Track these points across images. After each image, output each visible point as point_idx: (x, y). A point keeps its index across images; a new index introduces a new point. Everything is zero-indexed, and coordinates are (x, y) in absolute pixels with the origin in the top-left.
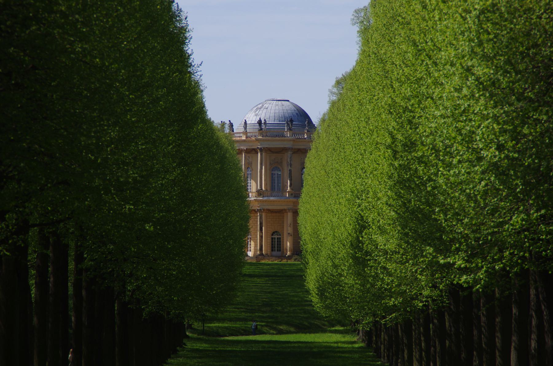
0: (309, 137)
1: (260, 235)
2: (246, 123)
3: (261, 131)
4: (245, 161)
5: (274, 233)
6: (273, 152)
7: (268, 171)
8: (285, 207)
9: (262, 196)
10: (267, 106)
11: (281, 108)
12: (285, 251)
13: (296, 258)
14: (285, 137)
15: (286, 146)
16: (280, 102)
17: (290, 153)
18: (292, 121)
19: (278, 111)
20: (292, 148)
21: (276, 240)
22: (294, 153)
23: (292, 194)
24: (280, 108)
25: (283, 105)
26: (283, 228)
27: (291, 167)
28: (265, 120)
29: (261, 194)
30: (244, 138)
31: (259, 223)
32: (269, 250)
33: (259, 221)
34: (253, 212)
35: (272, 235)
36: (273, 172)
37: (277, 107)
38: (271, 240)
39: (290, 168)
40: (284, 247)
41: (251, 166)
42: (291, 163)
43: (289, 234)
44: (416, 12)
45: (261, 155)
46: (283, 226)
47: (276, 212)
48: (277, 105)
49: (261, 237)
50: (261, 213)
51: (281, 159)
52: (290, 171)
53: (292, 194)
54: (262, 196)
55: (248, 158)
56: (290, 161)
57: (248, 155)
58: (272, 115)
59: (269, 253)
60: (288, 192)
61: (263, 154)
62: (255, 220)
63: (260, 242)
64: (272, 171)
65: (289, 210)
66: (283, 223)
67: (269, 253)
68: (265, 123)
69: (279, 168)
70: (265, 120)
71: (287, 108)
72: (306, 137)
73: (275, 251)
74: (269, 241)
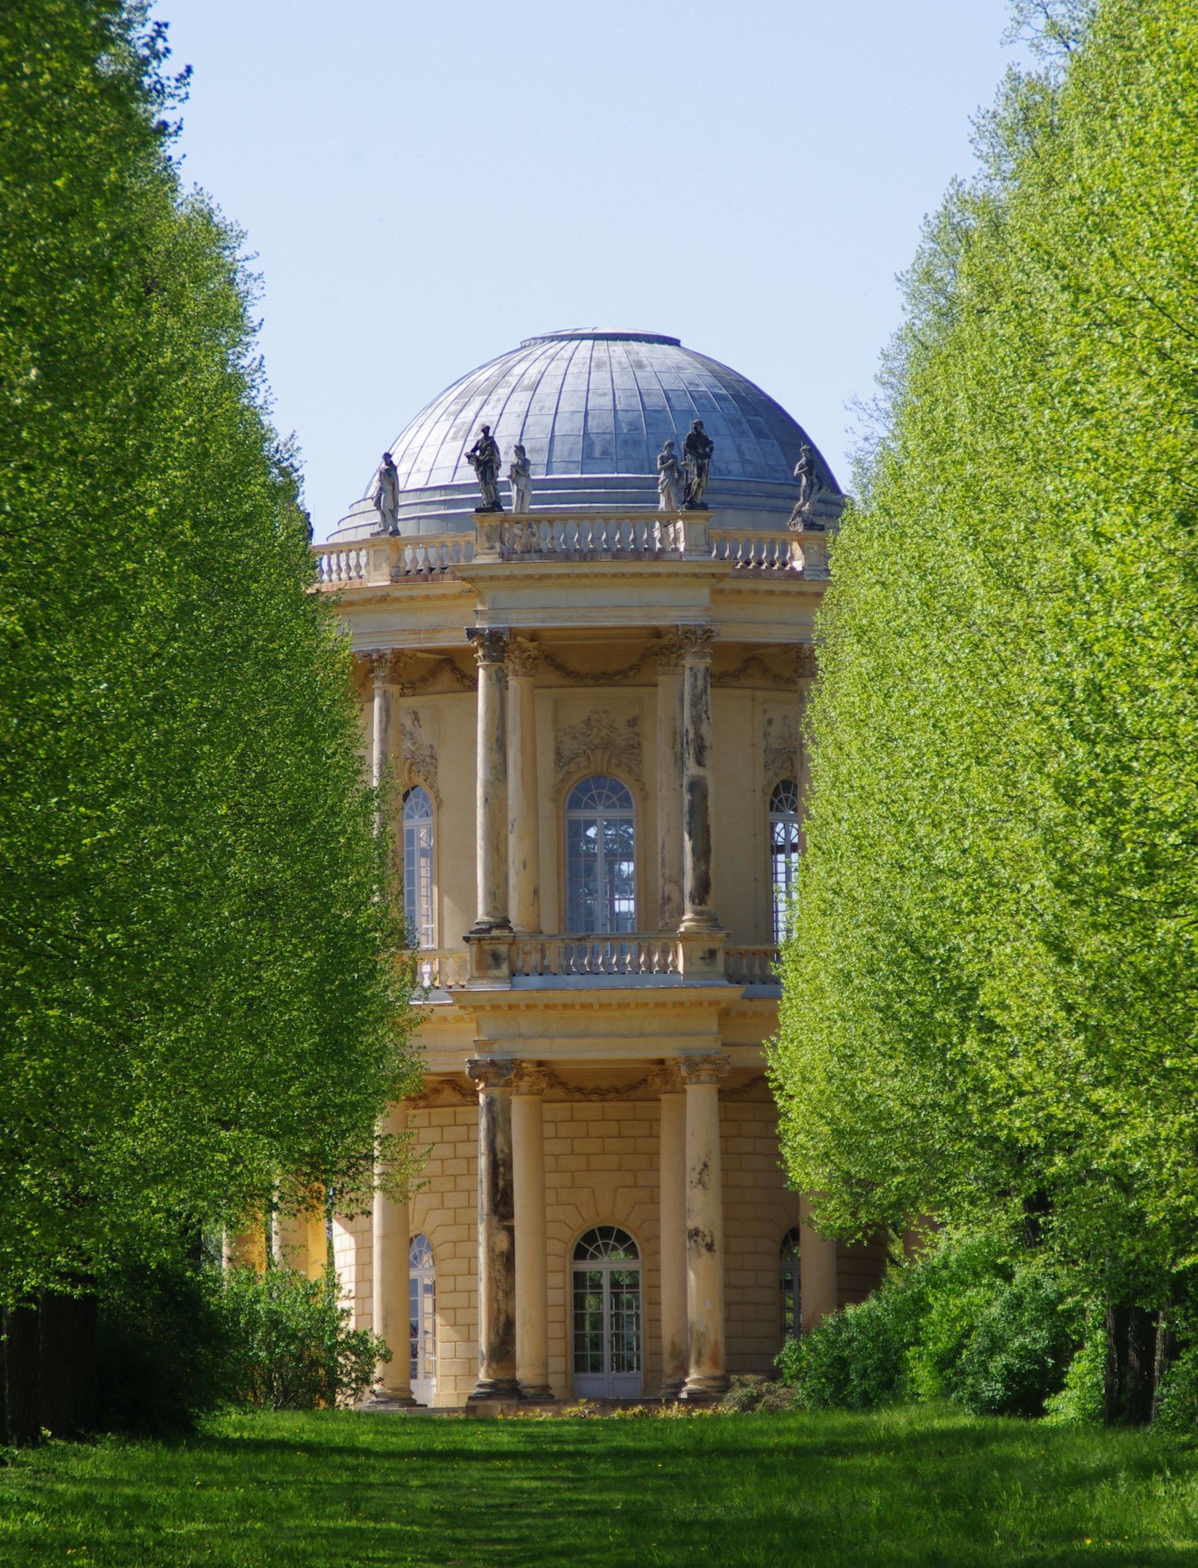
0: (819, 568)
1: (491, 1250)
2: (389, 472)
3: (493, 519)
4: (384, 741)
5: (589, 1237)
6: (575, 677)
7: (547, 808)
8: (668, 1050)
9: (505, 969)
10: (534, 372)
11: (631, 384)
12: (668, 1366)
13: (752, 1390)
14: (658, 556)
15: (663, 621)
16: (618, 348)
17: (694, 663)
18: (699, 444)
19: (607, 402)
20: (708, 634)
21: (607, 1353)
22: (718, 679)
23: (712, 954)
24: (624, 382)
25: (640, 365)
26: (654, 1201)
27: (700, 762)
28: (520, 450)
29: (496, 958)
30: (379, 580)
31: (483, 1162)
32: (559, 1364)
33: (483, 1146)
34: (448, 1095)
35: (580, 1253)
36: (586, 1266)
37: (600, 379)
38: (570, 1291)
39: (692, 769)
40: (656, 1320)
41: (430, 778)
42: (699, 737)
43: (695, 1234)
44: (1087, 747)
45: (499, 681)
46: (655, 1188)
47: (601, 1094)
48: (600, 365)
49: (505, 1261)
50: (497, 1092)
51: (633, 722)
52: (697, 788)
53: (712, 954)
54: (505, 969)
55: (407, 721)
56: (697, 721)
57: (410, 702)
58: (569, 426)
59: (556, 1382)
60: (686, 938)
61: (513, 682)
62: (463, 1149)
63: (492, 1299)
64: (575, 803)
65: (693, 1064)
66: (654, 1136)
67: (556, 1382)
68: (521, 468)
69: (616, 788)
70: (520, 450)
71: (669, 382)
72: (798, 565)
73: (597, 1367)
74: (560, 1293)
